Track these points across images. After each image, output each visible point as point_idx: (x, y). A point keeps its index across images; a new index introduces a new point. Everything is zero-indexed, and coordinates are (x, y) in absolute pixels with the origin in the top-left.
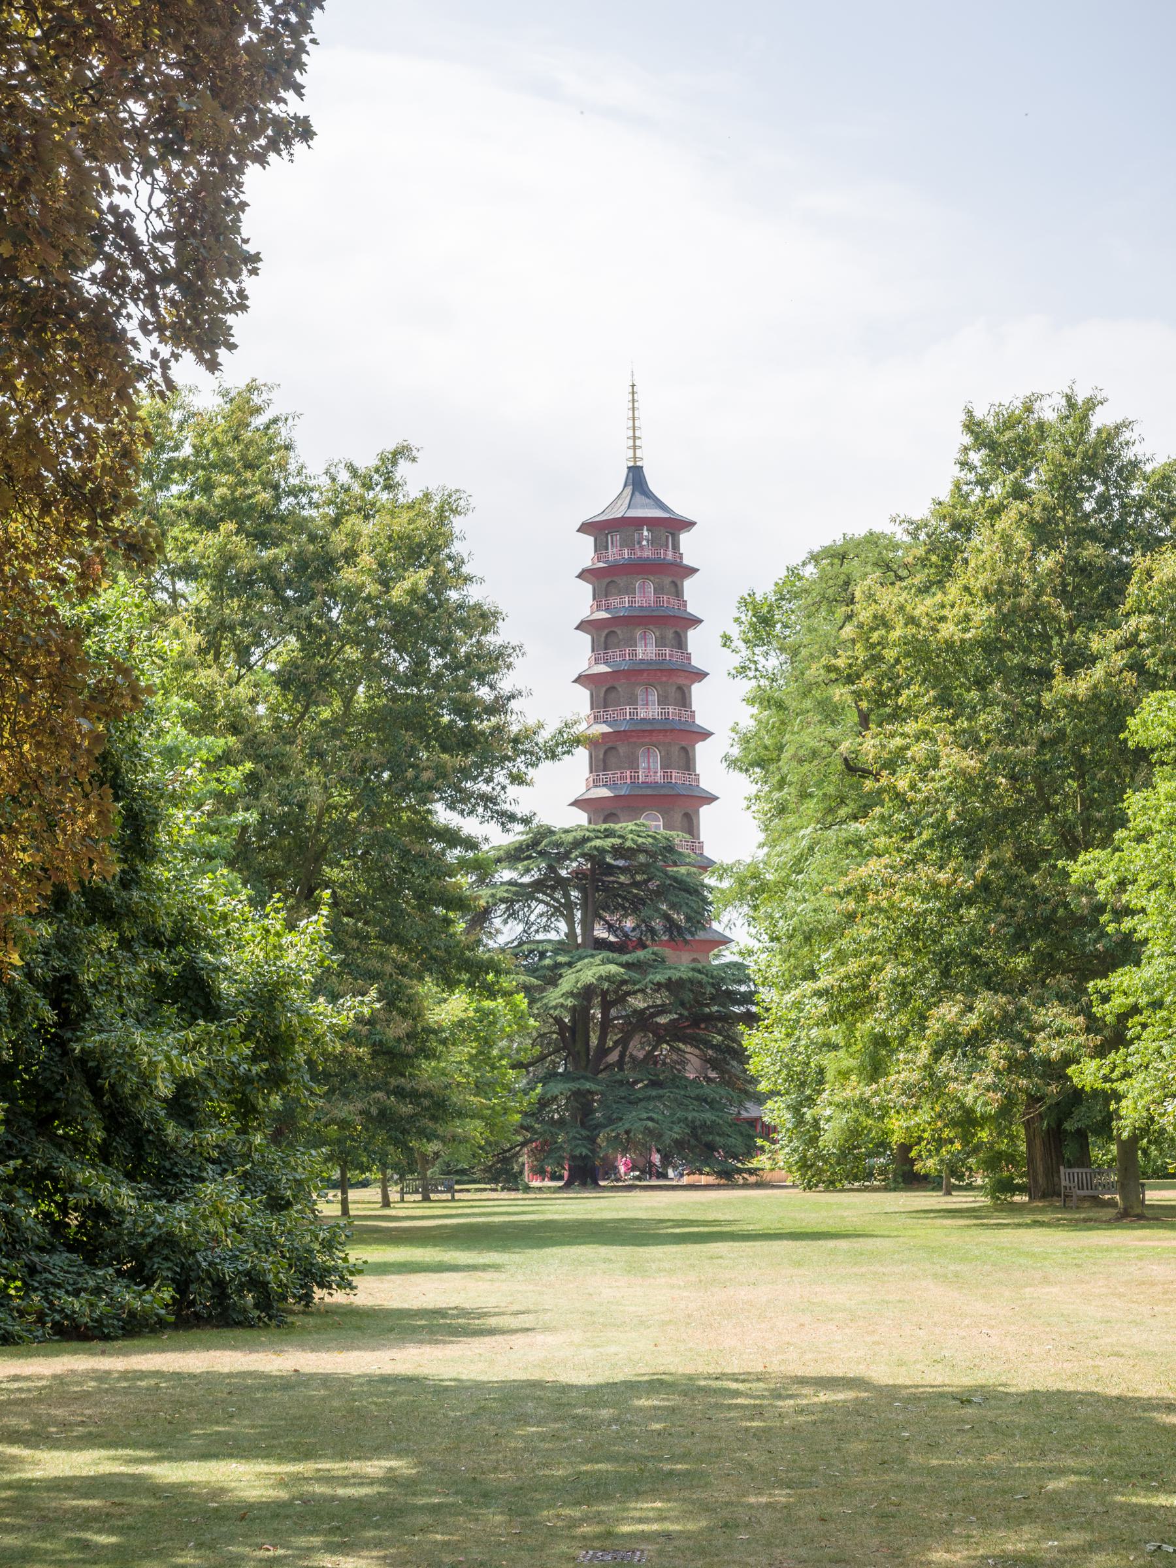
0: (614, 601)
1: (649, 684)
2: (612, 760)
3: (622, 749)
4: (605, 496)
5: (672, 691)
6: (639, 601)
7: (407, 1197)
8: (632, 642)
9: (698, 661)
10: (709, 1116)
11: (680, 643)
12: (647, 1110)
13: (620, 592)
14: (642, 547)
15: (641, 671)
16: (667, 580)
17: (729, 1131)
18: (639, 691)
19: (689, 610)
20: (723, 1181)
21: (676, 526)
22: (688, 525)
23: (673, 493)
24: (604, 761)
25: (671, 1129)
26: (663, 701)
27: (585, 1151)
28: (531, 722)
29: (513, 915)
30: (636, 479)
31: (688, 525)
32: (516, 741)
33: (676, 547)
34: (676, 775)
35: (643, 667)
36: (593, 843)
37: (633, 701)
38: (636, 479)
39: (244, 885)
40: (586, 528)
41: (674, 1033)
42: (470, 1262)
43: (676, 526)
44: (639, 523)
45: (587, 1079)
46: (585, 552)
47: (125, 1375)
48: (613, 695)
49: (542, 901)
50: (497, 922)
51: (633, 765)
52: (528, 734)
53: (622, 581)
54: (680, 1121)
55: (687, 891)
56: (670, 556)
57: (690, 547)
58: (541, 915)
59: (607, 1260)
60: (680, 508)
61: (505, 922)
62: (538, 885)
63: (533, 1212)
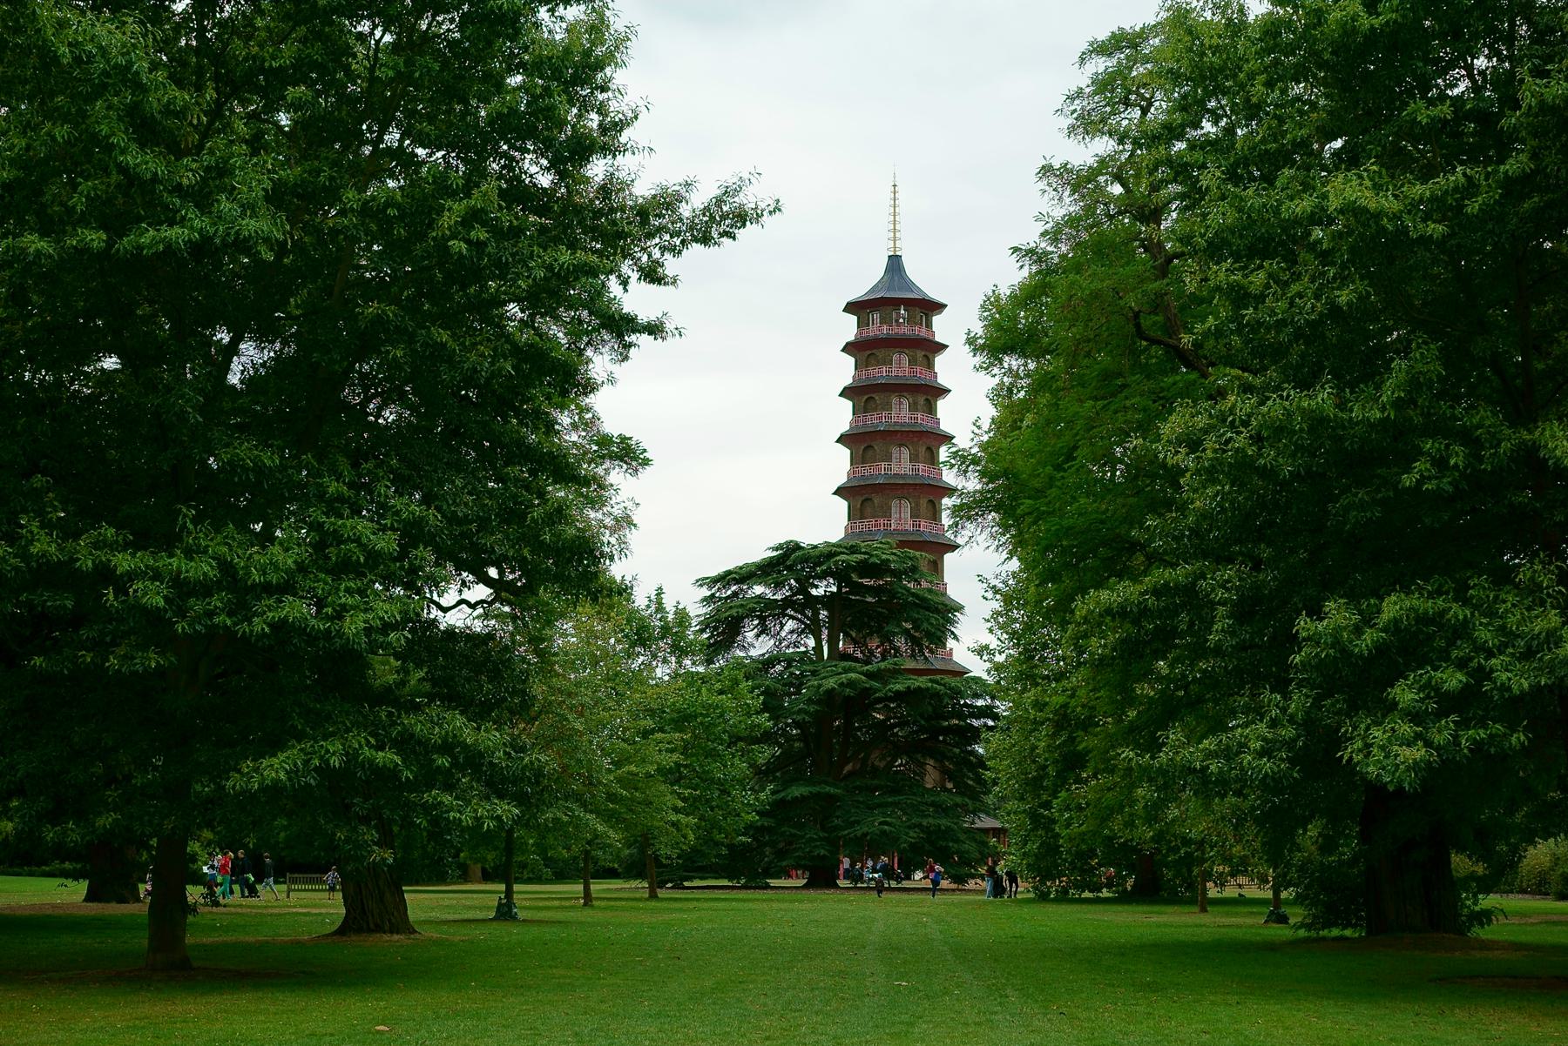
1: (900, 445)
2: (869, 510)
3: (877, 500)
4: (866, 279)
5: (922, 450)
7: (661, 893)
8: (887, 406)
9: (943, 380)
10: (944, 822)
11: (931, 409)
12: (885, 814)
13: (879, 363)
14: (899, 324)
15: (896, 432)
17: (962, 837)
19: (940, 381)
20: (954, 886)
22: (939, 307)
23: (925, 278)
24: (861, 510)
26: (914, 458)
27: (822, 852)
28: (672, 179)
29: (764, 630)
30: (895, 263)
31: (939, 307)
32: (643, 213)
33: (929, 325)
34: (924, 525)
37: (889, 458)
38: (895, 263)
40: (851, 308)
41: (914, 749)
44: (896, 303)
45: (826, 783)
46: (849, 328)
48: (870, 453)
49: (793, 618)
50: (750, 635)
51: (887, 514)
52: (666, 202)
53: (880, 353)
54: (915, 826)
55: (928, 609)
56: (923, 333)
58: (792, 632)
60: (934, 294)
61: (758, 636)
62: (787, 603)
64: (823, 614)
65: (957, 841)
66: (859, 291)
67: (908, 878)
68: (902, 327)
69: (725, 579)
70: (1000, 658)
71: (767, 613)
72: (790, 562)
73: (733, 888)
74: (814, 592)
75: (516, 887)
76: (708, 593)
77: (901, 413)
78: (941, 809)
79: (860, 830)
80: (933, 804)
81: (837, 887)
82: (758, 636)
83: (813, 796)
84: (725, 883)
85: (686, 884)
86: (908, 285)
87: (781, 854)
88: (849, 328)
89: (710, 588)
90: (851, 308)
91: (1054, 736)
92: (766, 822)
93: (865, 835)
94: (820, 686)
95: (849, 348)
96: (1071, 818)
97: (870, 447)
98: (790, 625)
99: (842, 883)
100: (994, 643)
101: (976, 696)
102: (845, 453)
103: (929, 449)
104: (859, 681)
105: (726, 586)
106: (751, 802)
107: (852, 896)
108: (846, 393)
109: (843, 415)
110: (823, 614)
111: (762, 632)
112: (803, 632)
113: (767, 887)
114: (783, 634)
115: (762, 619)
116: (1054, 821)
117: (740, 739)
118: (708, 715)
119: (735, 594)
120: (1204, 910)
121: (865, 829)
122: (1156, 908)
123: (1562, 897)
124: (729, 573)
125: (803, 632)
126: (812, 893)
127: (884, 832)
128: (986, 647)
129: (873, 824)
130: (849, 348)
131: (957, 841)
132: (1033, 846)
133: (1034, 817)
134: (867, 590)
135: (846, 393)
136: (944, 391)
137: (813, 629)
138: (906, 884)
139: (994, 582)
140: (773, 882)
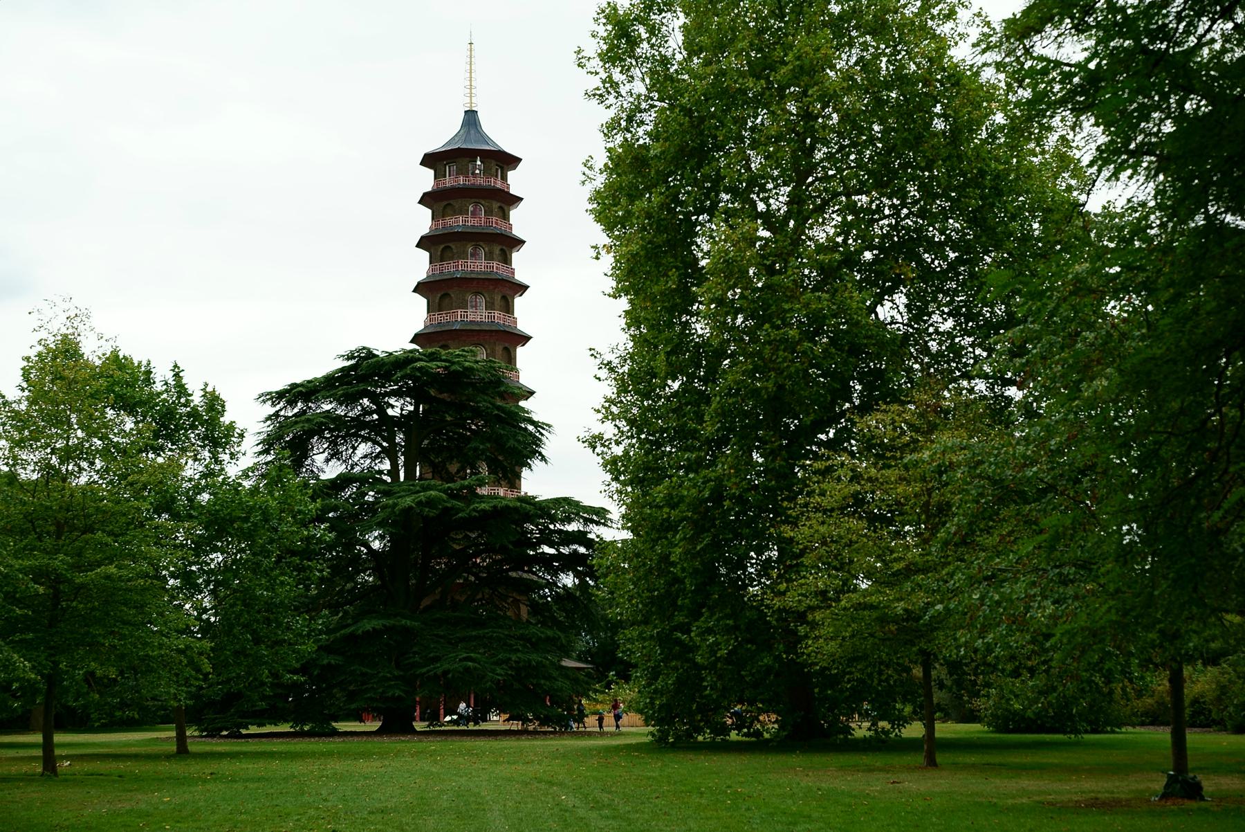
0: (450, 221)
1: (477, 293)
4: (442, 132)
5: (498, 298)
6: (471, 222)
10: (535, 658)
16: (496, 205)
17: (555, 674)
18: (469, 297)
20: (516, 726)
21: (509, 161)
22: (513, 161)
23: (500, 134)
25: (493, 671)
27: (398, 693)
29: (335, 455)
30: (471, 118)
31: (513, 161)
33: (504, 178)
35: (473, 276)
36: (418, 364)
38: (471, 118)
39: (906, 610)
42: (353, 729)
43: (509, 161)
44: (471, 154)
46: (426, 180)
47: (263, 725)
48: (447, 301)
50: (319, 459)
53: (457, 204)
56: (499, 185)
57: (516, 181)
58: (365, 456)
59: (470, 752)
61: (327, 461)
63: (22, 759)
64: (399, 438)
65: (549, 678)
66: (436, 143)
67: (485, 720)
68: (478, 176)
69: (292, 394)
70: (618, 451)
71: (341, 433)
72: (364, 373)
73: (302, 734)
74: (390, 412)
75: (58, 738)
76: (272, 411)
77: (477, 264)
78: (534, 644)
79: (441, 667)
80: (521, 637)
81: (413, 732)
82: (327, 461)
83: (387, 629)
84: (285, 728)
85: (244, 732)
86: (484, 138)
87: (352, 696)
88: (426, 180)
89: (273, 405)
90: (430, 160)
91: (693, 540)
92: (333, 660)
93: (445, 673)
94: (395, 505)
95: (424, 243)
96: (716, 643)
97: (446, 295)
98: (364, 448)
99: (419, 726)
100: (609, 430)
101: (569, 520)
102: (421, 302)
103: (506, 349)
104: (440, 500)
105: (291, 403)
106: (306, 635)
107: (433, 745)
108: (420, 288)
109: (420, 265)
110: (399, 438)
111: (332, 456)
112: (377, 456)
113: (335, 733)
114: (356, 459)
115: (333, 443)
116: (694, 649)
117: (293, 553)
118: (246, 520)
119: (303, 412)
120: (932, 763)
121: (446, 666)
122: (818, 759)
123: (1242, 729)
124: (294, 386)
125: (377, 456)
126: (388, 743)
127: (467, 669)
128: (599, 437)
129: (453, 662)
130: (424, 243)
131: (549, 678)
132: (668, 681)
133: (664, 640)
134: (453, 390)
135: (420, 288)
136: (519, 243)
137: (390, 453)
138: (484, 726)
139: (608, 357)
140: (343, 726)
